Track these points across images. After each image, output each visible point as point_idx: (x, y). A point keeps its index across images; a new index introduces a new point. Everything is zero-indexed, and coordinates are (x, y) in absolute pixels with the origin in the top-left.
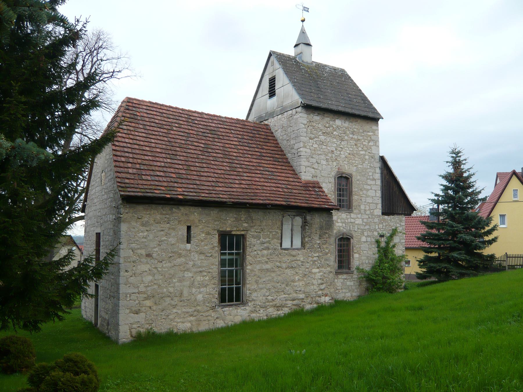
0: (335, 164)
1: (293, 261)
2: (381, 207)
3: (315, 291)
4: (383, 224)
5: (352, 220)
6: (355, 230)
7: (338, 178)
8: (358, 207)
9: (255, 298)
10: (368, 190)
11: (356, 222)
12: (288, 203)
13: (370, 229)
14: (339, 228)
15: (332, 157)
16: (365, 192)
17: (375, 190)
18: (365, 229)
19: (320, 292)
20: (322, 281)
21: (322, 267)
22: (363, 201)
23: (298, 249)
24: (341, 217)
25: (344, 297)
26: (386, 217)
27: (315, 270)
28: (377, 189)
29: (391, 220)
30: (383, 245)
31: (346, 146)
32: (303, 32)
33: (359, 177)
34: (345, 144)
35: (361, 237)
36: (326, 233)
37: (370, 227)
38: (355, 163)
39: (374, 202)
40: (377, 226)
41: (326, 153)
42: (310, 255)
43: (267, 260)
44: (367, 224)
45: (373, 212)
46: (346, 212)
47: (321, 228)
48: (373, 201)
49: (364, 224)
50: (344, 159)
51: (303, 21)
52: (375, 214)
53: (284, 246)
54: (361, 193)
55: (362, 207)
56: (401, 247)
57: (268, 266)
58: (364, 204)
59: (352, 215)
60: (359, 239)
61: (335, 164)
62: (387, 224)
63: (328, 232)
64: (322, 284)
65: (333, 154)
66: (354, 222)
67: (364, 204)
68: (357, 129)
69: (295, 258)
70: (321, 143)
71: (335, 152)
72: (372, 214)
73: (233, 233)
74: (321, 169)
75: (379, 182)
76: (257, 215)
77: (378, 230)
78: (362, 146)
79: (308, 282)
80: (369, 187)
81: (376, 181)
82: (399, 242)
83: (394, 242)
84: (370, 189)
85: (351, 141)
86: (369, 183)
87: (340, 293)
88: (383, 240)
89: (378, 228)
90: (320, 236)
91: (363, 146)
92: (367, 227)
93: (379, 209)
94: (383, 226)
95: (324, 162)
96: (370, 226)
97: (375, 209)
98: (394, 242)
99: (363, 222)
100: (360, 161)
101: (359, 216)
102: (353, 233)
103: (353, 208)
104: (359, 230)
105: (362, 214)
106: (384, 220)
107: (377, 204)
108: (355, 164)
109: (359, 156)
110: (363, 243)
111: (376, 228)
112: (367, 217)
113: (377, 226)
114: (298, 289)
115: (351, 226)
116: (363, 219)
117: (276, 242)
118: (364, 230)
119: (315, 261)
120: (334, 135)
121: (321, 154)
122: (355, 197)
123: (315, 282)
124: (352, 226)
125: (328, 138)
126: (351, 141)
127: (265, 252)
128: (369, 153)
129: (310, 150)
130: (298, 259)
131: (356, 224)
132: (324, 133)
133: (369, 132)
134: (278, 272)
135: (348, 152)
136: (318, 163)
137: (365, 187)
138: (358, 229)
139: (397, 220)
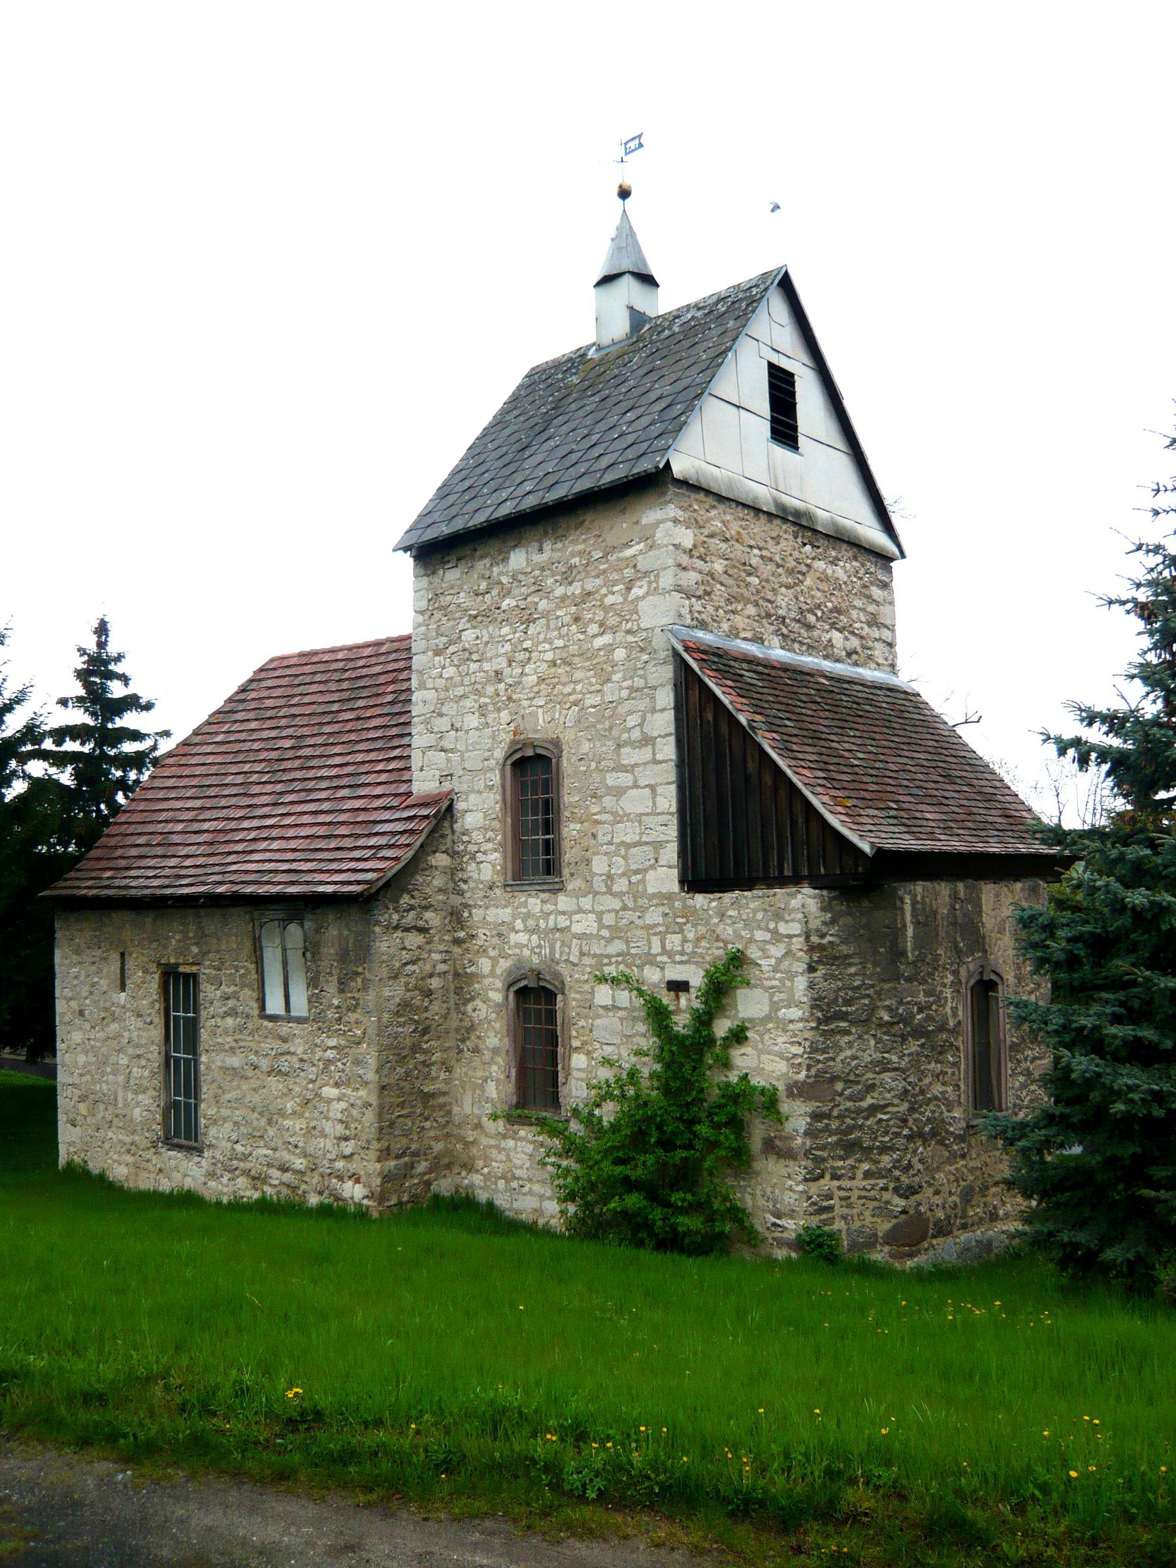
0: (505, 716)
1: (281, 1054)
2: (675, 855)
3: (328, 1156)
4: (682, 931)
5: (561, 918)
6: (571, 959)
7: (514, 764)
8: (582, 867)
9: (214, 1142)
10: (619, 792)
11: (576, 929)
12: (235, 888)
13: (628, 954)
14: (517, 951)
15: (498, 695)
16: (608, 801)
17: (652, 788)
18: (608, 956)
19: (340, 1164)
20: (346, 1128)
21: (347, 1083)
22: (602, 839)
23: (300, 1021)
24: (524, 910)
25: (536, 1210)
26: (700, 899)
27: (330, 1092)
28: (659, 780)
29: (722, 915)
30: (681, 1023)
31: (542, 637)
32: (626, 237)
33: (586, 747)
34: (538, 629)
35: (592, 988)
36: (357, 974)
37: (628, 946)
38: (574, 691)
39: (645, 839)
40: (655, 941)
41: (479, 686)
42: (318, 1041)
43: (233, 1044)
44: (617, 932)
45: (643, 881)
46: (543, 891)
47: (343, 956)
48: (641, 834)
49: (605, 933)
50: (536, 689)
51: (624, 194)
52: (651, 890)
53: (270, 1010)
54: (595, 809)
55: (599, 865)
56: (780, 1040)
57: (235, 1061)
58: (606, 854)
59: (563, 902)
60: (589, 996)
61: (505, 716)
62: (702, 930)
63: (360, 970)
64: (346, 1139)
65: (500, 681)
66: (568, 928)
67: (606, 854)
68: (580, 553)
69: (285, 1047)
70: (467, 655)
71: (507, 671)
72: (636, 892)
73: (181, 969)
74: (463, 748)
75: (668, 750)
76: (211, 923)
77: (659, 959)
78: (600, 615)
79: (313, 1123)
80: (625, 779)
81: (654, 745)
82: (768, 1019)
83: (741, 1015)
84: (630, 784)
85: (559, 613)
86: (625, 762)
87: (525, 1194)
88: (683, 1002)
89: (660, 950)
90: (340, 983)
91: (606, 612)
92: (617, 946)
93: (670, 867)
94: (685, 940)
95: (473, 721)
96: (627, 942)
97: (652, 867)
98: (741, 1015)
99: (601, 926)
100: (593, 680)
101: (586, 903)
102: (563, 969)
103: (566, 872)
104: (587, 961)
105: (596, 893)
106: (689, 913)
107: (658, 846)
108: (572, 698)
109: (588, 659)
110: (601, 1011)
111: (653, 951)
112: (617, 904)
113: (655, 941)
114: (291, 1140)
115: (558, 944)
116: (600, 915)
117: (248, 995)
118: (606, 961)
119: (329, 1062)
120: (504, 611)
121: (464, 696)
122: (572, 826)
123: (328, 1127)
124: (563, 942)
125: (485, 632)
126: (559, 613)
127: (230, 1021)
128: (629, 632)
129: (436, 690)
130: (292, 1049)
131: (578, 936)
132: (475, 617)
133: (627, 545)
134: (252, 1081)
135: (549, 656)
136: (457, 730)
137: (611, 779)
138: (582, 954)
139: (755, 911)
